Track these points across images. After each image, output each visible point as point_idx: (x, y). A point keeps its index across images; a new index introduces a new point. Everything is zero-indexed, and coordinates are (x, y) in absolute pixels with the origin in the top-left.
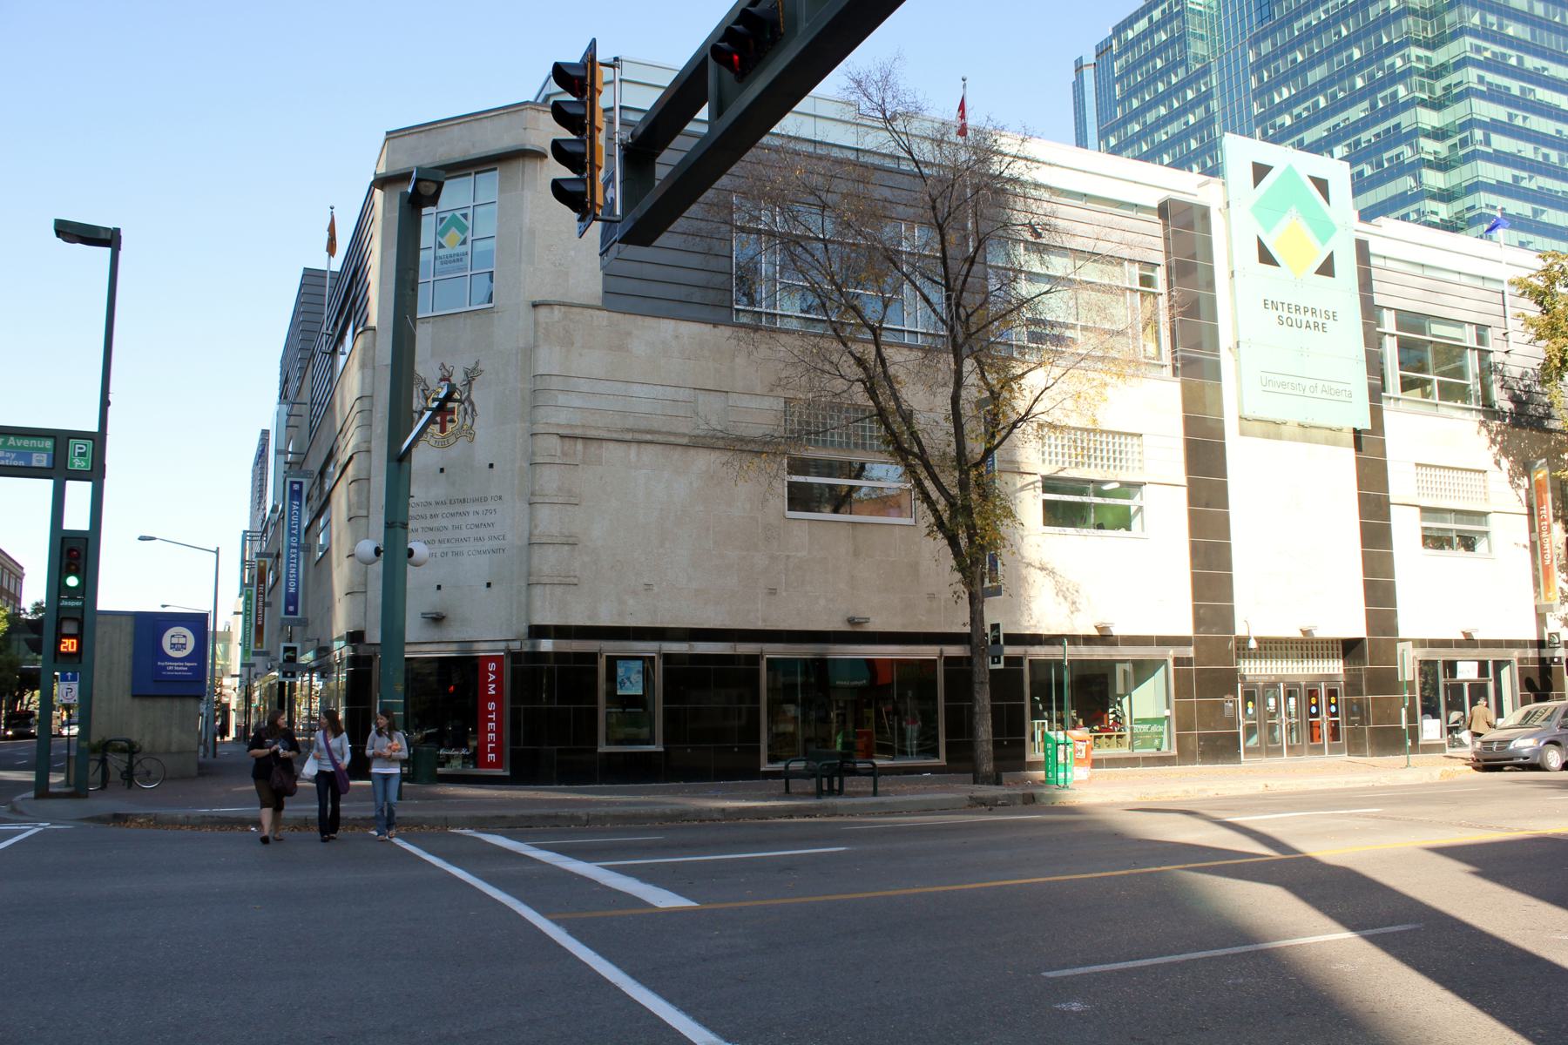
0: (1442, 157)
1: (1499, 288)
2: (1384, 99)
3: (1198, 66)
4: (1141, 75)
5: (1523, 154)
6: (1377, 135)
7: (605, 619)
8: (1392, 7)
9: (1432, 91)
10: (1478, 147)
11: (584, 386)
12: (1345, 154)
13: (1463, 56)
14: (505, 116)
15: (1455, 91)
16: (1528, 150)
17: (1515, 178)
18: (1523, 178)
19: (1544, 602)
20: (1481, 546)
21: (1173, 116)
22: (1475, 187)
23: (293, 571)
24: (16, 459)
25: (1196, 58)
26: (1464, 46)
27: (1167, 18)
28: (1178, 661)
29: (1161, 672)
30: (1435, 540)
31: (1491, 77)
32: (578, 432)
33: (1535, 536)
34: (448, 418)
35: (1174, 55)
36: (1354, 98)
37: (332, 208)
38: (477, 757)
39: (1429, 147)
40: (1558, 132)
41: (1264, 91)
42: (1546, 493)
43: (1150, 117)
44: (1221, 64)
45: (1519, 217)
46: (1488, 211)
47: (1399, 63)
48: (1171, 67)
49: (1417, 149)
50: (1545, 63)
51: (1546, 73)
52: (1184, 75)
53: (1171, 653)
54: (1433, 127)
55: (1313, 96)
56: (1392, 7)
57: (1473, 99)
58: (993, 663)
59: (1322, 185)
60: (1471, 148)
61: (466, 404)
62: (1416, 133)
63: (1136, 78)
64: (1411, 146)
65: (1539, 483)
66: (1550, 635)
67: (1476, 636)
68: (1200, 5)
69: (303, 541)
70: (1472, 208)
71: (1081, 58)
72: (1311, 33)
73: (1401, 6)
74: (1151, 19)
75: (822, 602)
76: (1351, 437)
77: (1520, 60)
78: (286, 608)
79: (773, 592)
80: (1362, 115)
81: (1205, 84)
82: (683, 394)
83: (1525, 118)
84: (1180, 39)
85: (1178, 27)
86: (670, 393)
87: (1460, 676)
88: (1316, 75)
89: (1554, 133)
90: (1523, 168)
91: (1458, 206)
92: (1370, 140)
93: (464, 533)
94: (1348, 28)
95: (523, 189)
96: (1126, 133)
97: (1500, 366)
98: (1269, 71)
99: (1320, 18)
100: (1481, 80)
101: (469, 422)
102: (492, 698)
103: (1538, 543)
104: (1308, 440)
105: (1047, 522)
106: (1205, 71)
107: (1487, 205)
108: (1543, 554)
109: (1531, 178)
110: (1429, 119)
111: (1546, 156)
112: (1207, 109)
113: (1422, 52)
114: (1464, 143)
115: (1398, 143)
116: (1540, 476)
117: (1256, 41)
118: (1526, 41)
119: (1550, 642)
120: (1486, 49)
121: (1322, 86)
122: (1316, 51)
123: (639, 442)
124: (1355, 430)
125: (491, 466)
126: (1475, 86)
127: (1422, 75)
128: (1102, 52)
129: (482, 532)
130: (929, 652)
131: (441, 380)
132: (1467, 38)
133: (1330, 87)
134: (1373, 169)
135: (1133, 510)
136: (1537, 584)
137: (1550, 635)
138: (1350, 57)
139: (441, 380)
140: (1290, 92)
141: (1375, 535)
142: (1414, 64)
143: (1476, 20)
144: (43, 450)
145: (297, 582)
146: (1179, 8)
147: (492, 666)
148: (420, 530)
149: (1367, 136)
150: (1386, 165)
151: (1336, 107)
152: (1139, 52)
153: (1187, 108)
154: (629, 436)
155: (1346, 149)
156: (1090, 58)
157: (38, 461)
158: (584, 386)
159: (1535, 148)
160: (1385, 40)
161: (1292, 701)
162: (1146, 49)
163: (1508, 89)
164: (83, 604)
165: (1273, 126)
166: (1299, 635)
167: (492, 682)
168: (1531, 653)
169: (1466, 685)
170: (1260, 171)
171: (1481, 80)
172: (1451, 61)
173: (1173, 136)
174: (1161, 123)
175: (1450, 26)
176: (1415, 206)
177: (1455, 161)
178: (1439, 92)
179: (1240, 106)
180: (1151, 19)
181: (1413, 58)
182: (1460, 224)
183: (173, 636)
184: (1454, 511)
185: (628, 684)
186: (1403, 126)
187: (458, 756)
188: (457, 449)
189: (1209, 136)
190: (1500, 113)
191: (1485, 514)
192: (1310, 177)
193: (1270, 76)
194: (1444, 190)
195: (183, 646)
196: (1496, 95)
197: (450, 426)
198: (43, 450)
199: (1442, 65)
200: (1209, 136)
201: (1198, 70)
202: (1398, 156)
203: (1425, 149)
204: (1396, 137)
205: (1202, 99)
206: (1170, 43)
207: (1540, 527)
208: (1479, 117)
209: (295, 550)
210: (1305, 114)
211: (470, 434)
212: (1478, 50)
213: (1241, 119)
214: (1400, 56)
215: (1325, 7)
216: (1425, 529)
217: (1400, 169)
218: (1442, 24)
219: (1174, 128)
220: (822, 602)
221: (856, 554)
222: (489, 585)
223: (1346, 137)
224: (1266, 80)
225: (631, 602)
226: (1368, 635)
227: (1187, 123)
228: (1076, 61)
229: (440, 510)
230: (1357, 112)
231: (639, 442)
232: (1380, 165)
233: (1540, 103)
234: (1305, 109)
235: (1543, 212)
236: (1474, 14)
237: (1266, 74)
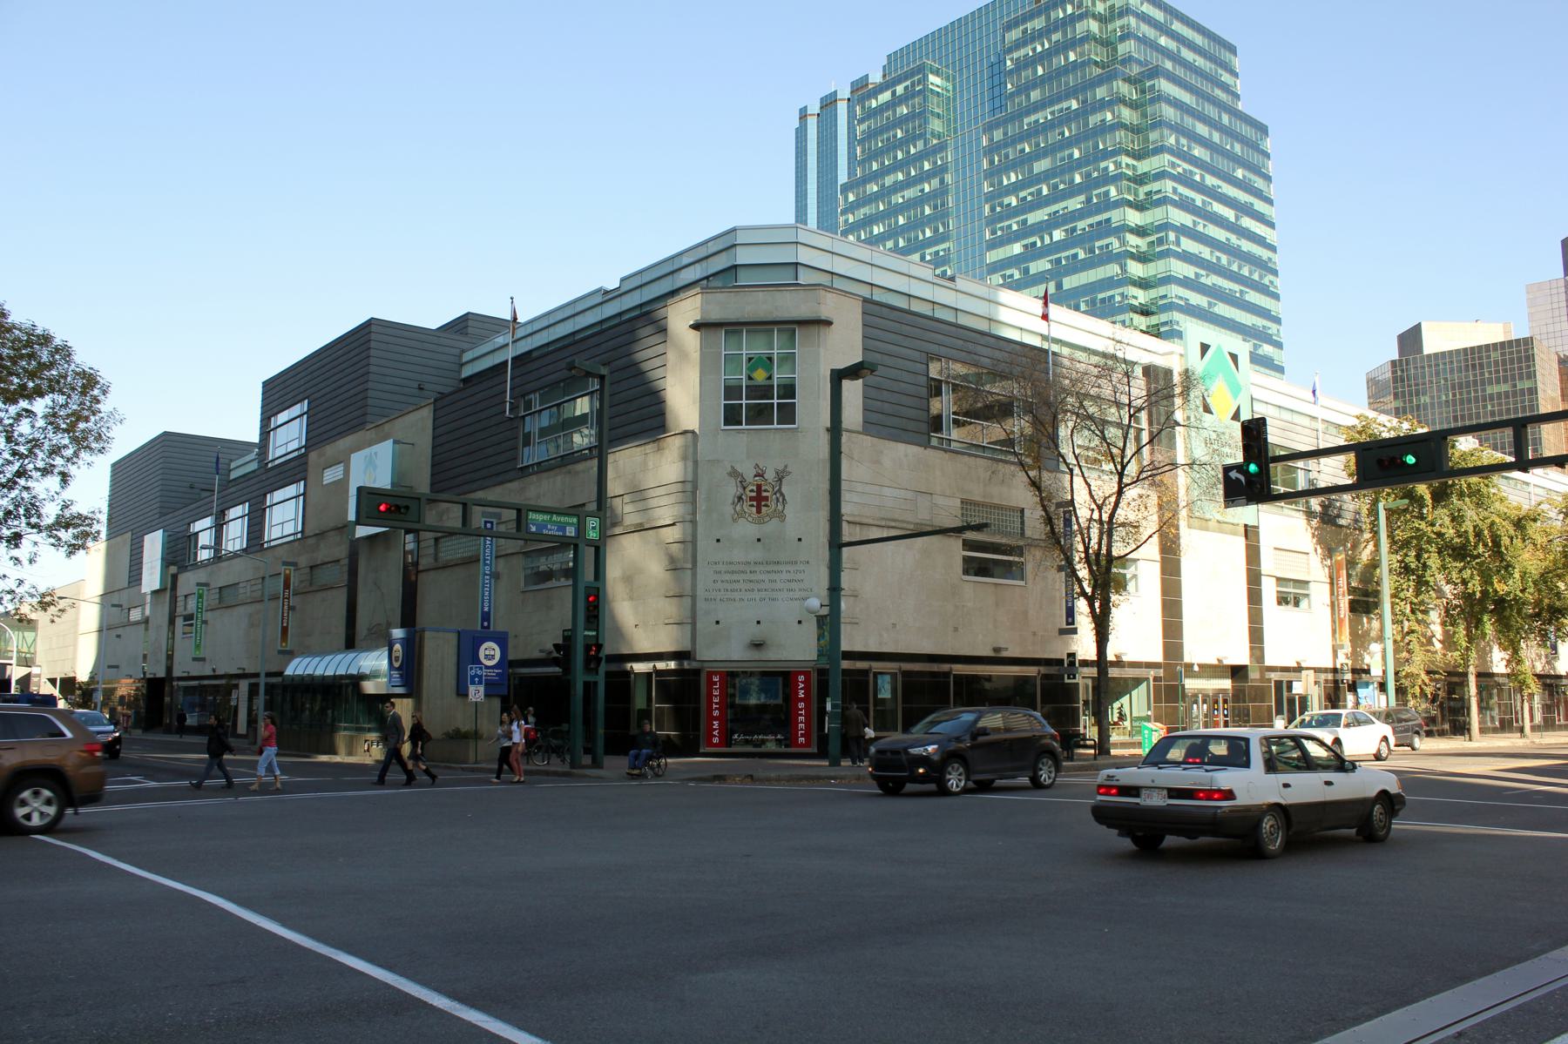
0: (1142, 250)
1: (1314, 425)
2: (1098, 196)
3: (935, 142)
4: (882, 141)
5: (1203, 256)
6: (1091, 226)
7: (873, 648)
8: (1108, 119)
9: (1136, 195)
10: (1171, 247)
11: (859, 488)
12: (1063, 238)
13: (1162, 169)
14: (802, 292)
15: (1155, 198)
16: (1205, 252)
17: (1197, 274)
18: (1202, 276)
19: (1338, 643)
20: (1304, 603)
21: (909, 183)
22: (1168, 280)
23: (487, 594)
24: (557, 530)
25: (933, 134)
26: (1161, 161)
27: (909, 95)
28: (1156, 679)
29: (1144, 686)
30: (1282, 600)
31: (1181, 189)
32: (857, 519)
33: (1334, 598)
34: (763, 503)
35: (914, 128)
36: (1073, 191)
37: (512, 298)
38: (791, 740)
39: (1133, 240)
40: (1228, 239)
41: (994, 173)
42: (1343, 569)
43: (889, 181)
44: (956, 142)
45: (1198, 307)
46: (1177, 301)
47: (1112, 167)
48: (910, 139)
49: (1123, 243)
50: (1220, 183)
51: (1220, 190)
52: (922, 148)
53: (1152, 673)
54: (1136, 225)
55: (1037, 184)
56: (1108, 119)
57: (1169, 207)
58: (1069, 678)
59: (1234, 357)
60: (1166, 247)
61: (778, 495)
62: (1125, 228)
63: (877, 144)
64: (1119, 238)
65: (1338, 563)
66: (1342, 665)
67: (1125, 659)
68: (938, 86)
69: (493, 569)
70: (1165, 297)
71: (806, 107)
72: (1037, 130)
73: (1116, 121)
74: (894, 93)
75: (980, 637)
76: (1243, 529)
77: (1202, 177)
78: (482, 624)
79: (956, 629)
80: (1079, 206)
81: (942, 159)
82: (909, 495)
83: (1205, 226)
84: (920, 115)
85: (920, 104)
86: (903, 493)
87: (1294, 692)
88: (1041, 166)
89: (1224, 241)
90: (1203, 268)
91: (1153, 293)
92: (1085, 229)
93: (779, 585)
94: (1070, 130)
95: (819, 346)
96: (865, 192)
97: (1315, 481)
98: (1000, 156)
99: (1046, 118)
100: (1175, 190)
101: (780, 507)
102: (801, 700)
103: (1336, 603)
104: (1222, 531)
105: (966, 572)
106: (942, 147)
107: (1176, 296)
108: (1339, 610)
109: (1207, 276)
110: (1134, 218)
111: (1218, 259)
112: (942, 181)
113: (1130, 161)
114: (1160, 241)
115: (1108, 235)
116: (1339, 558)
117: (989, 128)
118: (1206, 162)
119: (1342, 670)
120: (1179, 166)
121: (1045, 176)
122: (1042, 145)
123: (889, 527)
124: (1246, 526)
125: (800, 540)
126: (1171, 196)
127: (1129, 179)
128: (826, 105)
129: (793, 585)
130: (1031, 671)
131: (755, 476)
132: (1166, 155)
133: (1054, 178)
134: (1085, 254)
135: (1128, 576)
136: (1334, 632)
137: (1342, 665)
138: (1071, 156)
139: (755, 476)
140: (1017, 177)
141: (1254, 597)
142: (1124, 170)
143: (1172, 140)
144: (571, 524)
145: (490, 602)
146: (921, 87)
147: (801, 678)
148: (742, 581)
149: (1081, 225)
150: (1097, 252)
151: (1056, 196)
152: (882, 120)
153: (924, 177)
154: (883, 523)
155: (1063, 233)
156: (815, 108)
157: (570, 532)
158: (859, 488)
159: (1211, 252)
160: (1101, 147)
161: (1205, 706)
162: (888, 118)
163: (1194, 200)
164: (598, 634)
165: (1001, 205)
166: (1216, 662)
167: (801, 689)
168: (1330, 676)
169: (1297, 697)
170: (1205, 348)
171: (1175, 190)
172: (1153, 172)
173: (909, 199)
174: (898, 187)
175: (1154, 142)
176: (1120, 290)
177: (1154, 255)
178: (1142, 197)
179: (972, 183)
180: (894, 93)
181: (1124, 166)
182: (1154, 309)
183: (486, 649)
184: (1293, 580)
185: (883, 691)
186: (1113, 221)
187: (772, 740)
188: (772, 526)
189: (943, 205)
190: (1186, 219)
191: (1307, 582)
192: (1230, 353)
193: (1000, 161)
194: (1142, 279)
195: (493, 657)
196: (1185, 205)
197: (764, 509)
198: (571, 524)
199: (1145, 173)
200: (943, 205)
201: (936, 145)
202: (1107, 246)
203: (1130, 243)
204: (1105, 229)
205: (939, 171)
206: (911, 117)
207: (1338, 592)
208: (1172, 222)
209: (488, 577)
210: (1029, 198)
211: (781, 516)
212: (1173, 165)
213: (972, 194)
214: (1113, 162)
215: (1052, 109)
216: (1278, 592)
217: (1108, 257)
218: (1146, 140)
219: (910, 193)
220: (980, 637)
221: (997, 605)
222: (800, 622)
223: (1064, 223)
224: (996, 163)
225: (885, 635)
226: (1251, 663)
227: (922, 191)
228: (801, 110)
229: (757, 568)
230: (1075, 203)
231: (889, 527)
232: (1092, 251)
233: (1215, 214)
234: (1030, 194)
235: (1215, 304)
236: (1171, 136)
237: (996, 159)
